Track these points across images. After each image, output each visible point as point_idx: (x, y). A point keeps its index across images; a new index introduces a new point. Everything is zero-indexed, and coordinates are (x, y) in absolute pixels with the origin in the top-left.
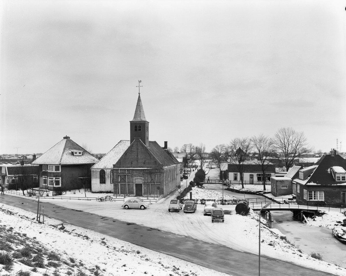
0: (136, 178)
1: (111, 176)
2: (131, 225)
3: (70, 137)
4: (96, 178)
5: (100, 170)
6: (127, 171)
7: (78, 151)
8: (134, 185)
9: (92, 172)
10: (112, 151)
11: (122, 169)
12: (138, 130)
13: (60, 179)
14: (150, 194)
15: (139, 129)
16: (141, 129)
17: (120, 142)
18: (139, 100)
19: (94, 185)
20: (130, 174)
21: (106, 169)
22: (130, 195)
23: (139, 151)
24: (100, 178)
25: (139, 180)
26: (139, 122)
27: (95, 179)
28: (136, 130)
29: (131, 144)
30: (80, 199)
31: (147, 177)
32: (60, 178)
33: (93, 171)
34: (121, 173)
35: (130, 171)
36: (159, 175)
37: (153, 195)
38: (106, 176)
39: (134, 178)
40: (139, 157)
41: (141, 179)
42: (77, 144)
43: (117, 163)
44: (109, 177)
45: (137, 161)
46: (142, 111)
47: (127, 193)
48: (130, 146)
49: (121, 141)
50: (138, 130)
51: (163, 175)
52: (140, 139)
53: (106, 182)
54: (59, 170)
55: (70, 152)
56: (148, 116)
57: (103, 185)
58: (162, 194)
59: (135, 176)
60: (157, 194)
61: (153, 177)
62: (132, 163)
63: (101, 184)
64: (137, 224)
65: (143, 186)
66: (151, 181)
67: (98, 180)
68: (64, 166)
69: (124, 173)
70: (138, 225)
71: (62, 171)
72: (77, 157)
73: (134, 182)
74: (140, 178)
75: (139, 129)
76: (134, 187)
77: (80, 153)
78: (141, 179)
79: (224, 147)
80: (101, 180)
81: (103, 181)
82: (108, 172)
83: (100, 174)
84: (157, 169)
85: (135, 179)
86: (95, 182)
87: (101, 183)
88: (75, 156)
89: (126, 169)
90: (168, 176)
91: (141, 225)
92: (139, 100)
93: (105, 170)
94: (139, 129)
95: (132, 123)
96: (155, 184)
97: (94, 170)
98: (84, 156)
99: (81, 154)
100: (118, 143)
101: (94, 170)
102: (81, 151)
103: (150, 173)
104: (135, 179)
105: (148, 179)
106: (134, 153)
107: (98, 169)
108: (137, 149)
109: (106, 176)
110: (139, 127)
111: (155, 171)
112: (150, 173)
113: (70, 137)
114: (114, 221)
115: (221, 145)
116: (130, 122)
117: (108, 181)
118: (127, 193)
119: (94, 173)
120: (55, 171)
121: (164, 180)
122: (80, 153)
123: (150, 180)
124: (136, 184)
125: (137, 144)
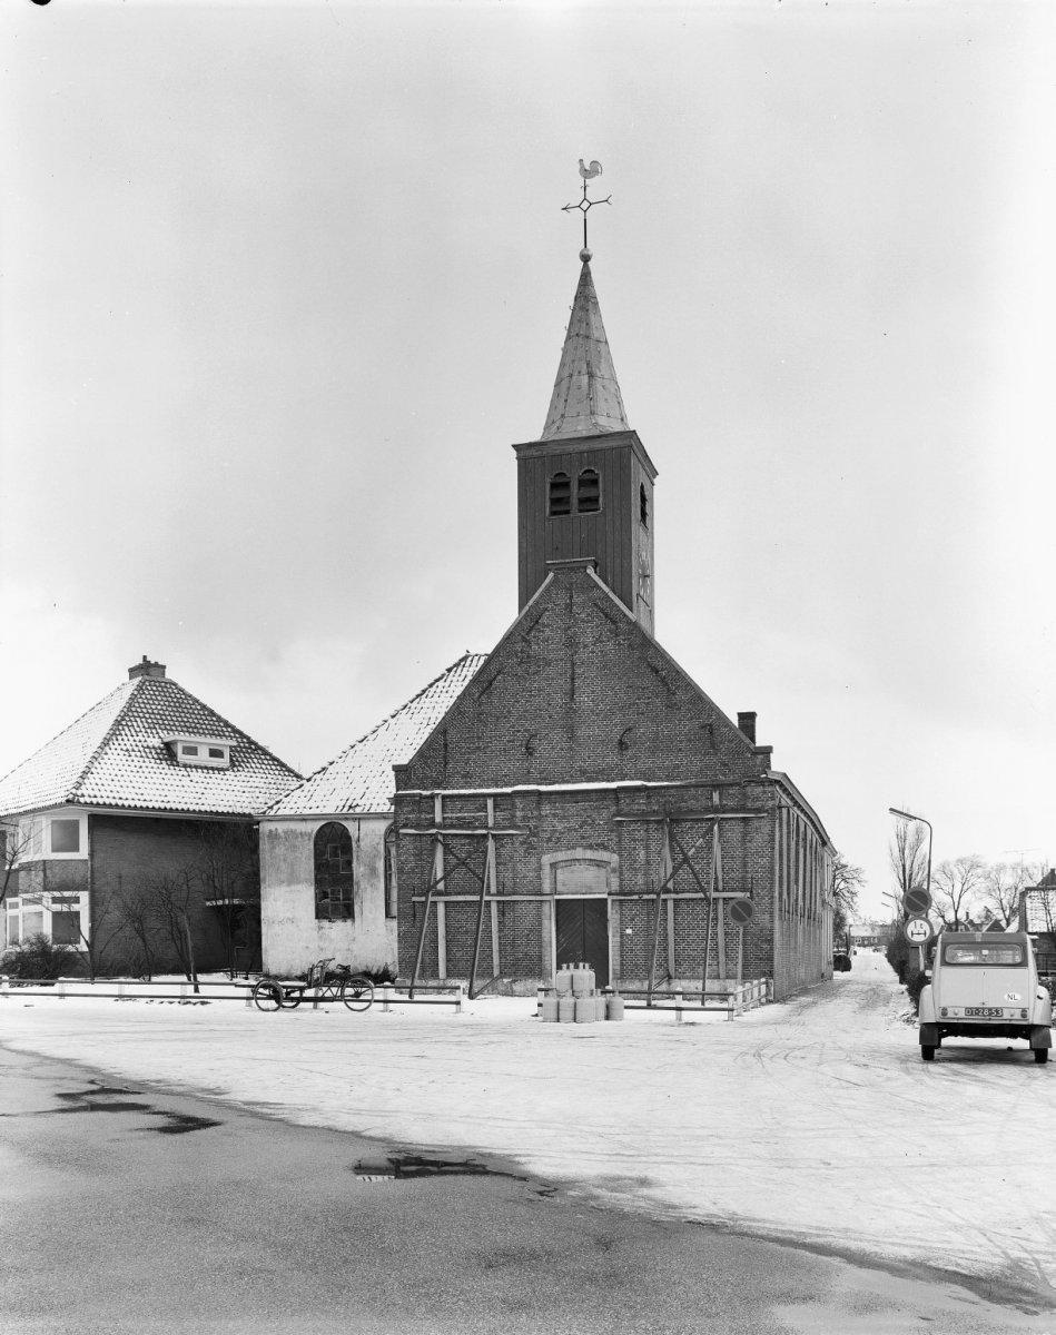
0: (561, 856)
1: (388, 867)
2: (486, 1180)
3: (164, 667)
4: (292, 880)
5: (317, 825)
6: (496, 807)
7: (204, 743)
8: (546, 908)
9: (264, 846)
10: (403, 716)
11: (456, 792)
12: (575, 501)
13: (83, 906)
14: (670, 977)
15: (582, 498)
16: (596, 500)
17: (457, 665)
18: (585, 297)
19: (277, 928)
20: (518, 828)
21: (359, 818)
22: (518, 987)
23: (583, 655)
24: (318, 882)
25: (582, 874)
26: (585, 447)
27: (284, 888)
28: (559, 506)
29: (521, 607)
30: (131, 997)
31: (647, 847)
32: (84, 896)
33: (273, 836)
34: (452, 826)
35: (517, 801)
36: (735, 831)
37: (693, 985)
38: (354, 864)
39: (547, 859)
40: (584, 699)
41: (599, 864)
42: (204, 707)
43: (422, 754)
44: (373, 871)
45: (571, 732)
46: (602, 371)
47: (496, 972)
48: (518, 626)
49: (464, 659)
50: (575, 501)
51: (766, 829)
52: (590, 571)
53: (357, 909)
54: (76, 848)
55: (156, 742)
56: (644, 403)
57: (338, 929)
58: (764, 974)
59: (556, 842)
60: (718, 977)
61: (693, 842)
62: (530, 751)
63: (325, 923)
64: (544, 1166)
65: (613, 915)
66: (676, 870)
67: (306, 896)
68: (111, 823)
69: (469, 825)
70: (549, 1189)
71: (92, 854)
72: (197, 775)
73: (547, 887)
74: (589, 854)
75: (582, 498)
76: (546, 922)
77: (215, 753)
78: (599, 864)
79: (979, 871)
80: (321, 895)
81: (335, 900)
82: (369, 837)
83: (318, 854)
84: (717, 786)
85: (554, 866)
86: (289, 923)
87: (321, 913)
88: (185, 766)
89: (490, 795)
90: (793, 877)
91: (614, 1183)
92: (585, 297)
93: (351, 827)
94: (582, 501)
95: (528, 456)
96: (706, 899)
97: (281, 827)
98: (242, 775)
99: (224, 762)
100: (449, 670)
101: (281, 827)
102: (225, 743)
103: (669, 816)
104: (554, 866)
105: (648, 862)
106: (550, 671)
107: (304, 819)
108: (572, 643)
109: (359, 870)
110: (582, 483)
111: (704, 802)
112: (669, 816)
113: (164, 667)
114: (185, 1124)
115: (961, 861)
116: (514, 453)
117: (371, 899)
118: (496, 972)
119: (280, 850)
120: (55, 849)
121: (777, 868)
122: (215, 753)
123: (670, 871)
124: (558, 901)
125: (569, 606)
